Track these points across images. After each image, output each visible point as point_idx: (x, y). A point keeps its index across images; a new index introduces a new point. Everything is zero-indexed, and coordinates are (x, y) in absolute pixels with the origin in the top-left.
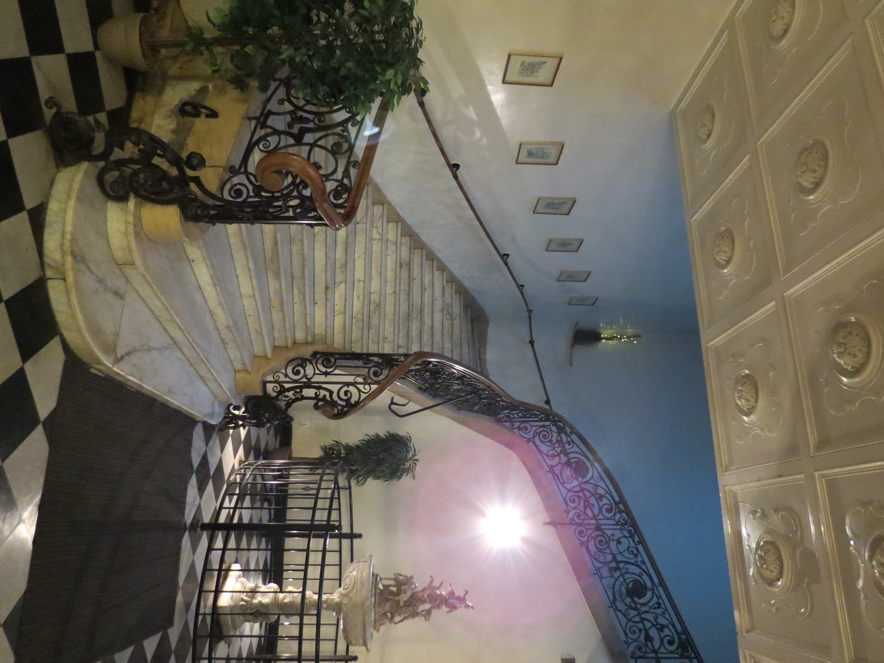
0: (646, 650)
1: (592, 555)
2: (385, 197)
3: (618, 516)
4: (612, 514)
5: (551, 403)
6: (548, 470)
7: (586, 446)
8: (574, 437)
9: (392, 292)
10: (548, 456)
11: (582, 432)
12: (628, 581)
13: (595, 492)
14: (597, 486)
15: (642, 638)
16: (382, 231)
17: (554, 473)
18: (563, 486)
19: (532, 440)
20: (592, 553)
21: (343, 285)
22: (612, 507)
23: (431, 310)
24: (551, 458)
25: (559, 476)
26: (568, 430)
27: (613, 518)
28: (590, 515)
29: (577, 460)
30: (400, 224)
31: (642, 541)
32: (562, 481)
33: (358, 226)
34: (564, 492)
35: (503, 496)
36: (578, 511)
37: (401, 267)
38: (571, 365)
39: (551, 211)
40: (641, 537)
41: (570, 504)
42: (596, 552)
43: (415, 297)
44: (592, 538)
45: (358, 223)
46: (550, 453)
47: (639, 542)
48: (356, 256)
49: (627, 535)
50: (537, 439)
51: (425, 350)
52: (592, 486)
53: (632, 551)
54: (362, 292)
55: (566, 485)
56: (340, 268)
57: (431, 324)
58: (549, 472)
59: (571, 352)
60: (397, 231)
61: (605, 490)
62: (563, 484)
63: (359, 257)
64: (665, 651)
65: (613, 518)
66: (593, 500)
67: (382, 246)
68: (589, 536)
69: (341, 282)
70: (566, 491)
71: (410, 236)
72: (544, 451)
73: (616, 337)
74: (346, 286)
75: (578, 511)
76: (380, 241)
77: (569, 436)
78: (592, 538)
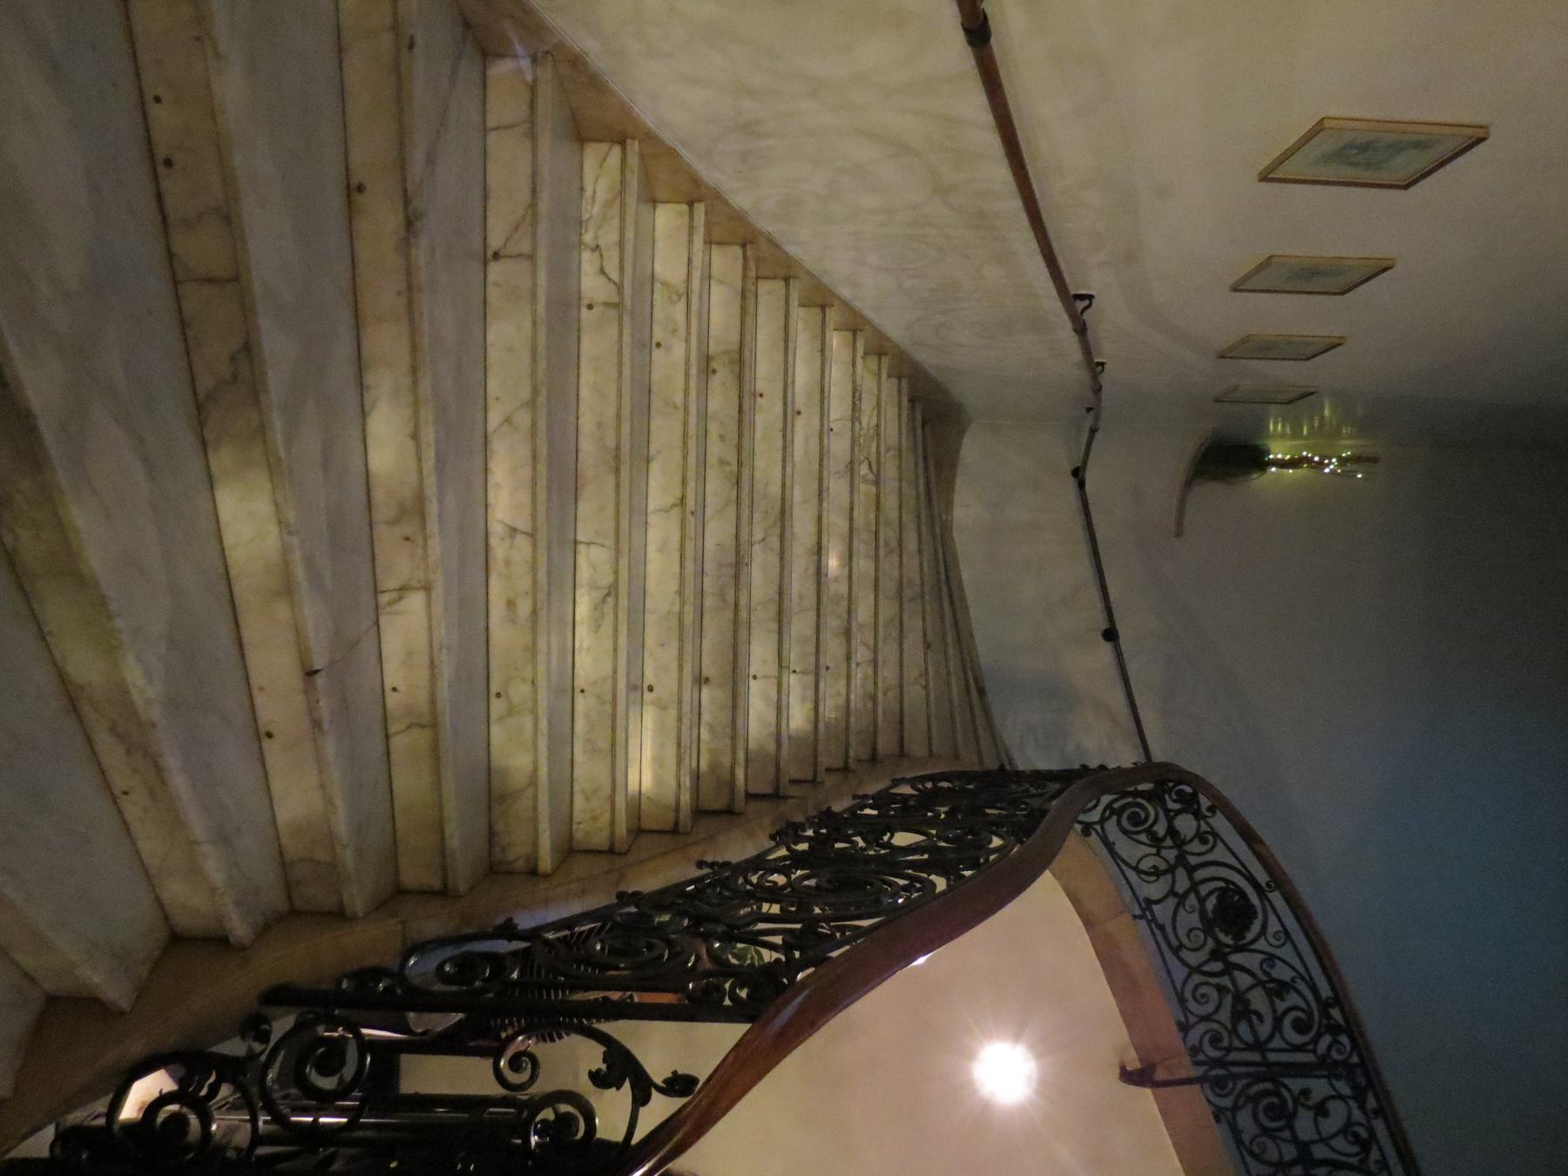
0: (1231, 1043)
1: (1243, 1144)
2: (626, 111)
3: (1326, 1040)
4: (1306, 1038)
5: (1121, 640)
6: (1138, 912)
7: (1251, 847)
8: (1220, 822)
9: (671, 500)
10: (1139, 872)
11: (1240, 806)
12: (1204, 889)
13: (1267, 974)
14: (1271, 959)
15: (1224, 1015)
16: (622, 268)
17: (1154, 919)
18: (1179, 958)
19: (1098, 827)
20: (1246, 1138)
21: (416, 601)
22: (1310, 1014)
23: (815, 485)
24: (1146, 878)
25: (1169, 930)
26: (1205, 802)
27: (1311, 1047)
28: (1249, 1038)
29: (1221, 884)
30: (700, 208)
31: (1385, 1111)
32: (1175, 943)
33: (495, 269)
34: (1180, 973)
35: (1017, 1038)
36: (1215, 1026)
37: (707, 369)
38: (1179, 534)
39: (1349, 173)
40: (1384, 1097)
41: (1192, 1005)
42: (1256, 1136)
43: (760, 463)
44: (1250, 1099)
45: (496, 256)
46: (1146, 865)
47: (1379, 1112)
48: (494, 419)
49: (1346, 1091)
50: (1111, 825)
51: (797, 821)
52: (1260, 957)
53: (1356, 1135)
54: (525, 583)
55: (1184, 954)
56: (394, 522)
57: (814, 540)
58: (1141, 917)
59: (1182, 501)
60: (690, 242)
61: (1294, 968)
62: (1175, 951)
63: (508, 420)
64: (1284, 1046)
65: (1311, 1047)
66: (1258, 999)
67: (621, 335)
68: (1239, 1096)
69: (404, 589)
70: (1186, 971)
71: (744, 246)
72: (1124, 855)
73: (1309, 460)
74: (429, 604)
75: (1215, 1026)
76: (613, 313)
77: (1204, 817)
78: (1250, 1099)
